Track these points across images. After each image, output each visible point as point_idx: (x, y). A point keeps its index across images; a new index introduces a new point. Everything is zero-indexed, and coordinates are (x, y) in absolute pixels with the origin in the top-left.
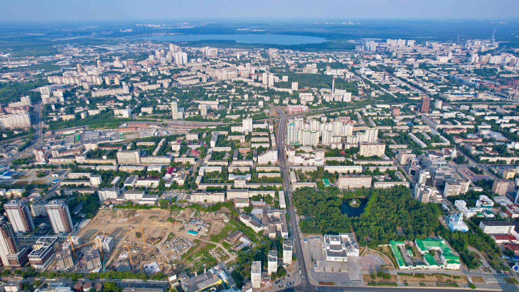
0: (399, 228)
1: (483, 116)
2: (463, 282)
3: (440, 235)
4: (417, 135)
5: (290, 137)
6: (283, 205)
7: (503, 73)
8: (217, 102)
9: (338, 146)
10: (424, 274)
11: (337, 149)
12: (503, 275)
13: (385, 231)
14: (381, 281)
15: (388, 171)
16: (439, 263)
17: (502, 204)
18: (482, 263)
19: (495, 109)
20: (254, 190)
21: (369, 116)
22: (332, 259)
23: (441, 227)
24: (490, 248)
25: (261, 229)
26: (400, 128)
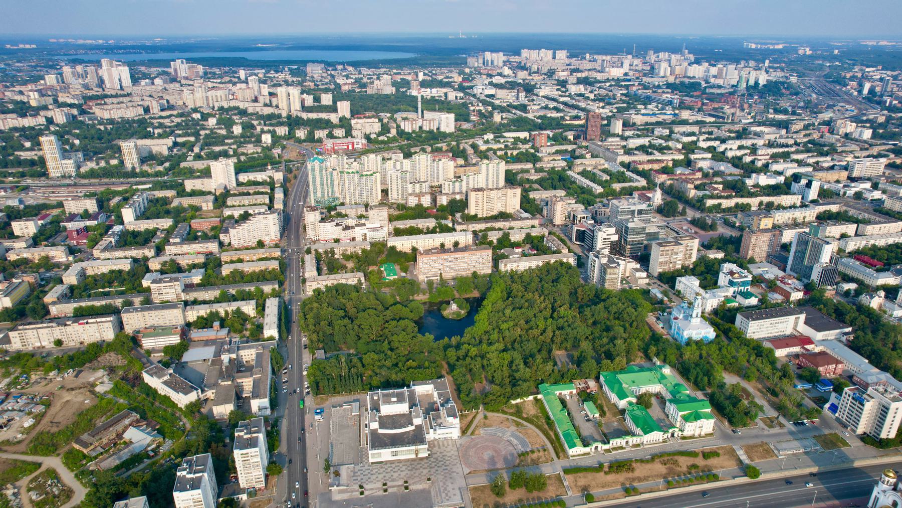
0: (559, 354)
1: (695, 143)
2: (726, 463)
3: (657, 355)
4: (584, 174)
5: (315, 188)
6: (271, 331)
7: (710, 87)
8: (169, 141)
9: (423, 199)
11: (419, 206)
12: (808, 430)
13: (526, 363)
14: (520, 500)
15: (529, 239)
16: (665, 425)
17: (767, 276)
18: (761, 408)
19: (710, 133)
20: (204, 302)
21: (489, 149)
22: (385, 454)
23: (656, 338)
24: (767, 370)
25: (193, 397)
26: (548, 166)
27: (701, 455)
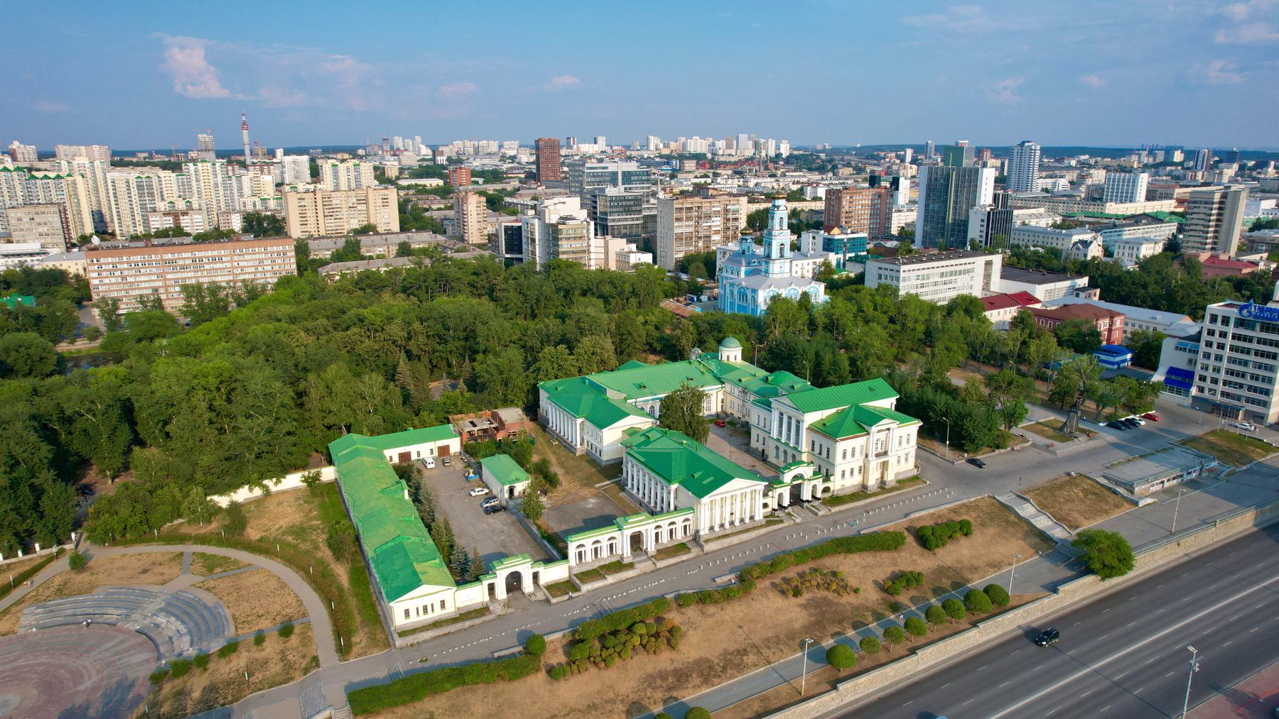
10: (660, 601)
27: (910, 540)
